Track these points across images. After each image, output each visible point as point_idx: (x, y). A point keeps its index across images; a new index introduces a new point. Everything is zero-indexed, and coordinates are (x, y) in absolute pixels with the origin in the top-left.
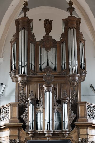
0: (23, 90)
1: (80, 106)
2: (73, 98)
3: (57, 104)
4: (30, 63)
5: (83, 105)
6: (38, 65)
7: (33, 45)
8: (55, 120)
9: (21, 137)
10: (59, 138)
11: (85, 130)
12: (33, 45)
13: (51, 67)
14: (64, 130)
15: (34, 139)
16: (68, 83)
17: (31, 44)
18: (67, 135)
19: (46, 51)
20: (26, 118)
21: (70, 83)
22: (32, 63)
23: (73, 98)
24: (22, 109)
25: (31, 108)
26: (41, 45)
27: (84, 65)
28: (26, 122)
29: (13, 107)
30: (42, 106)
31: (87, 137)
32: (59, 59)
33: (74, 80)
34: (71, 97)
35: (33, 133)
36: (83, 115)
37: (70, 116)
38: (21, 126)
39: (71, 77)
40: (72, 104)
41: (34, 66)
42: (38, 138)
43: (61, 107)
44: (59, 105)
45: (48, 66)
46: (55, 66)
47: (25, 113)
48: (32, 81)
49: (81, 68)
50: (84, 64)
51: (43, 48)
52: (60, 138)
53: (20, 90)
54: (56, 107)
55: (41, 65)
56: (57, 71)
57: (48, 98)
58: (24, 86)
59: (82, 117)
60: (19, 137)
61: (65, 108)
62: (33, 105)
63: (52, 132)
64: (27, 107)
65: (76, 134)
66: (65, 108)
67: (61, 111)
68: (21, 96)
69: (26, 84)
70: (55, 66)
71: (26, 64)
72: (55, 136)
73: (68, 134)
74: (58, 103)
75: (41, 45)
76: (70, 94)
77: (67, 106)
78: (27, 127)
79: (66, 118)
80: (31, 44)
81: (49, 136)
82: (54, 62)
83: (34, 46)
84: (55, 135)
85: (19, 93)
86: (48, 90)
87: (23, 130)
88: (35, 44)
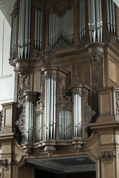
0: (23, 82)
1: (103, 95)
2: (95, 84)
3: (65, 98)
4: (34, 40)
5: (107, 93)
6: (46, 40)
7: (39, 12)
8: (60, 123)
9: (17, 155)
10: (70, 152)
11: (108, 136)
12: (39, 12)
13: (66, 41)
14: (75, 138)
15: (81, 153)
16: (88, 59)
17: (36, 11)
18: (80, 146)
19: (59, 16)
20: (22, 125)
21: (91, 60)
22: (38, 40)
23: (95, 84)
24: (17, 111)
25: (27, 106)
26: (52, 10)
27: (115, 27)
28: (22, 131)
29: (6, 110)
30: (42, 102)
31: (115, 148)
32: (77, 25)
33: (95, 54)
34: (92, 82)
35: (30, 147)
36: (107, 110)
37: (84, 114)
38: (12, 137)
39: (89, 49)
40: (94, 94)
41: (41, 44)
42: (39, 155)
43: (71, 101)
44: (69, 97)
45: (62, 39)
46: (71, 37)
47: (21, 117)
48: (35, 68)
49: (108, 32)
50: (114, 24)
51: (55, 14)
52: (71, 152)
53: (20, 83)
54: (64, 101)
55: (51, 39)
56: (74, 45)
57: (50, 90)
58: (25, 76)
59: (105, 115)
60: (13, 154)
61: (78, 101)
62: (31, 103)
63: (54, 144)
64: (24, 107)
65: (96, 144)
66: (78, 101)
67: (70, 107)
68: (21, 92)
69: (28, 72)
70: (71, 38)
71: (26, 43)
72: (64, 151)
73: (82, 145)
74: (66, 95)
75: (52, 10)
76: (91, 78)
77: (80, 98)
78: (23, 139)
79: (78, 118)
80: (36, 11)
81: (49, 151)
82: (70, 33)
83: (41, 13)
84: (64, 148)
85: (19, 88)
86: (50, 76)
87: (17, 144)
88: (42, 11)
